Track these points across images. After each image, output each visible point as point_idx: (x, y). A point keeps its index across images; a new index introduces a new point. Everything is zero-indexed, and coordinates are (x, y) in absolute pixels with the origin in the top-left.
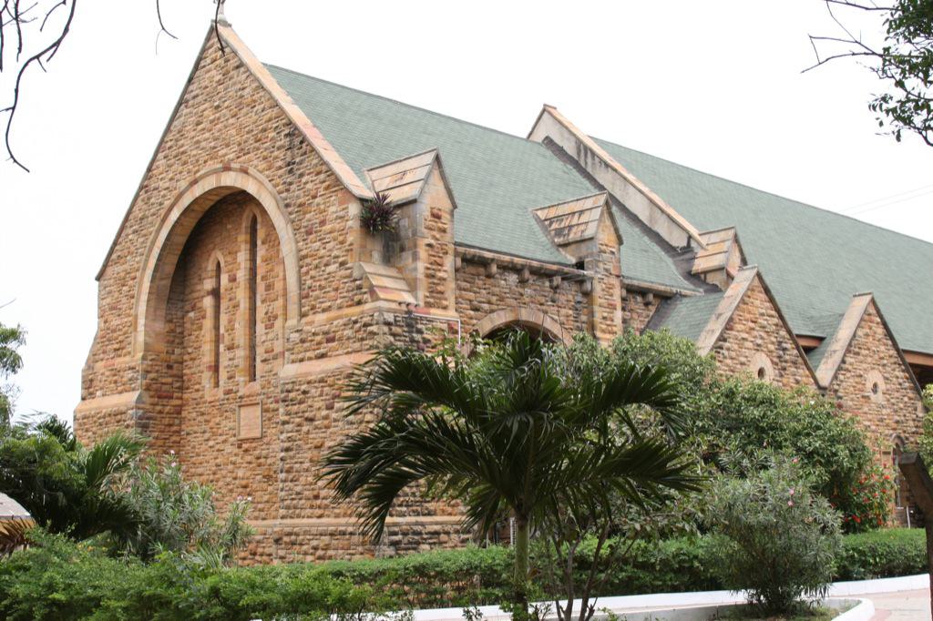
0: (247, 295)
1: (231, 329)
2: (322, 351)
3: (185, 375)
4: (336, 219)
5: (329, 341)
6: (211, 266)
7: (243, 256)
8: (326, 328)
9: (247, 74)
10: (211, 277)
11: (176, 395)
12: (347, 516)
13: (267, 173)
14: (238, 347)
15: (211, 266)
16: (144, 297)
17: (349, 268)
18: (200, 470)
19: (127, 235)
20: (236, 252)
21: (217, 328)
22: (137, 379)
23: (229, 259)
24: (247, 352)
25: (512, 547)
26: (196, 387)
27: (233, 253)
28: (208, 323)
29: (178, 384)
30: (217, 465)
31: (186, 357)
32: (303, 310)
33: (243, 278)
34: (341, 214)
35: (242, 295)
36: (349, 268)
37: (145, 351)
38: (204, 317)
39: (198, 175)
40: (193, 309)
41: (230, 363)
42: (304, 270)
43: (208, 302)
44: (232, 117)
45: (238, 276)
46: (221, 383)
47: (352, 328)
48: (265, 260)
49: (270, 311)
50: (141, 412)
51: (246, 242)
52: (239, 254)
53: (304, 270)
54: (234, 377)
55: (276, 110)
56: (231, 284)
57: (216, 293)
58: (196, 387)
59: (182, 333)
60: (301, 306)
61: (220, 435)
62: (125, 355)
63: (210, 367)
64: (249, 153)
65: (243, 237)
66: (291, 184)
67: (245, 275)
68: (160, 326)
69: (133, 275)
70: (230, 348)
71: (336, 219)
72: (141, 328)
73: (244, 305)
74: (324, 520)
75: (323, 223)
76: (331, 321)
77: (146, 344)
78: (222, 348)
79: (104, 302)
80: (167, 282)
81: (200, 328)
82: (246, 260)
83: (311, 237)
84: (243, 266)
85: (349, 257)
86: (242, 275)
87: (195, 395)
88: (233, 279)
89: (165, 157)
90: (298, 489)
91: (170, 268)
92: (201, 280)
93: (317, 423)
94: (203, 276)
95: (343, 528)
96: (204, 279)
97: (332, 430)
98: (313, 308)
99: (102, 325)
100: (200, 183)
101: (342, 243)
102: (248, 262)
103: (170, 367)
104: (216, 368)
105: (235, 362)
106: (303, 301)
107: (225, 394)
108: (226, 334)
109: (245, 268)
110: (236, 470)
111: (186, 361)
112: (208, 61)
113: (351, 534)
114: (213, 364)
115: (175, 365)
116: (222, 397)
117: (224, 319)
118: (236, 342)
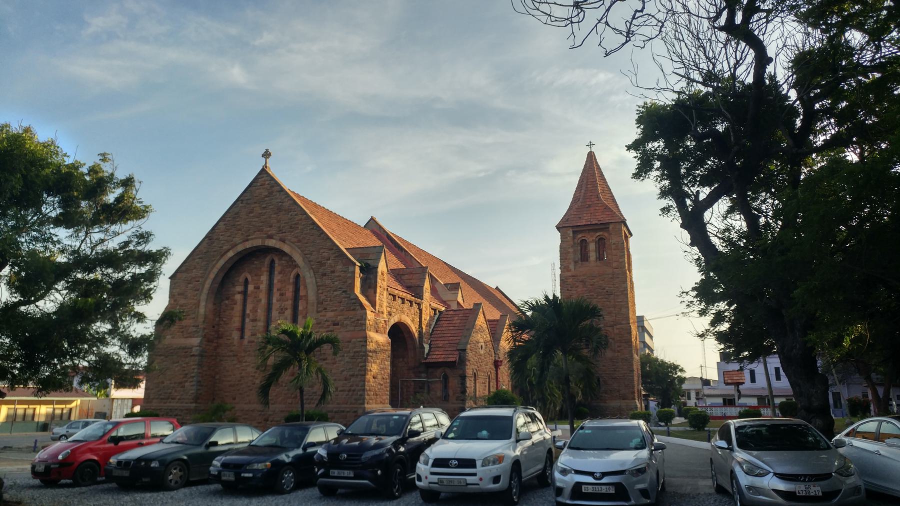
1: (255, 310)
6: (241, 279)
7: (264, 278)
12: (172, 432)
13: (297, 244)
14: (259, 321)
15: (241, 279)
16: (205, 291)
19: (194, 259)
20: (261, 275)
21: (244, 310)
22: (199, 332)
23: (255, 278)
25: (409, 427)
27: (258, 276)
28: (238, 308)
30: (241, 377)
31: (221, 322)
38: (235, 304)
39: (249, 238)
40: (227, 299)
42: (320, 291)
43: (239, 297)
45: (261, 287)
51: (267, 271)
52: (262, 277)
53: (320, 291)
55: (304, 216)
56: (256, 290)
57: (245, 293)
60: (318, 307)
64: (285, 233)
65: (265, 269)
66: (313, 251)
68: (211, 306)
69: (197, 279)
70: (254, 320)
73: (264, 301)
75: (333, 272)
77: (205, 315)
78: (247, 320)
79: (174, 291)
80: (217, 285)
81: (233, 309)
84: (265, 282)
86: (264, 286)
88: (257, 288)
90: (315, 390)
92: (234, 286)
94: (236, 284)
97: (337, 365)
99: (172, 302)
112: (259, 184)
113: (348, 412)
114: (240, 327)
117: (249, 307)
118: (258, 318)
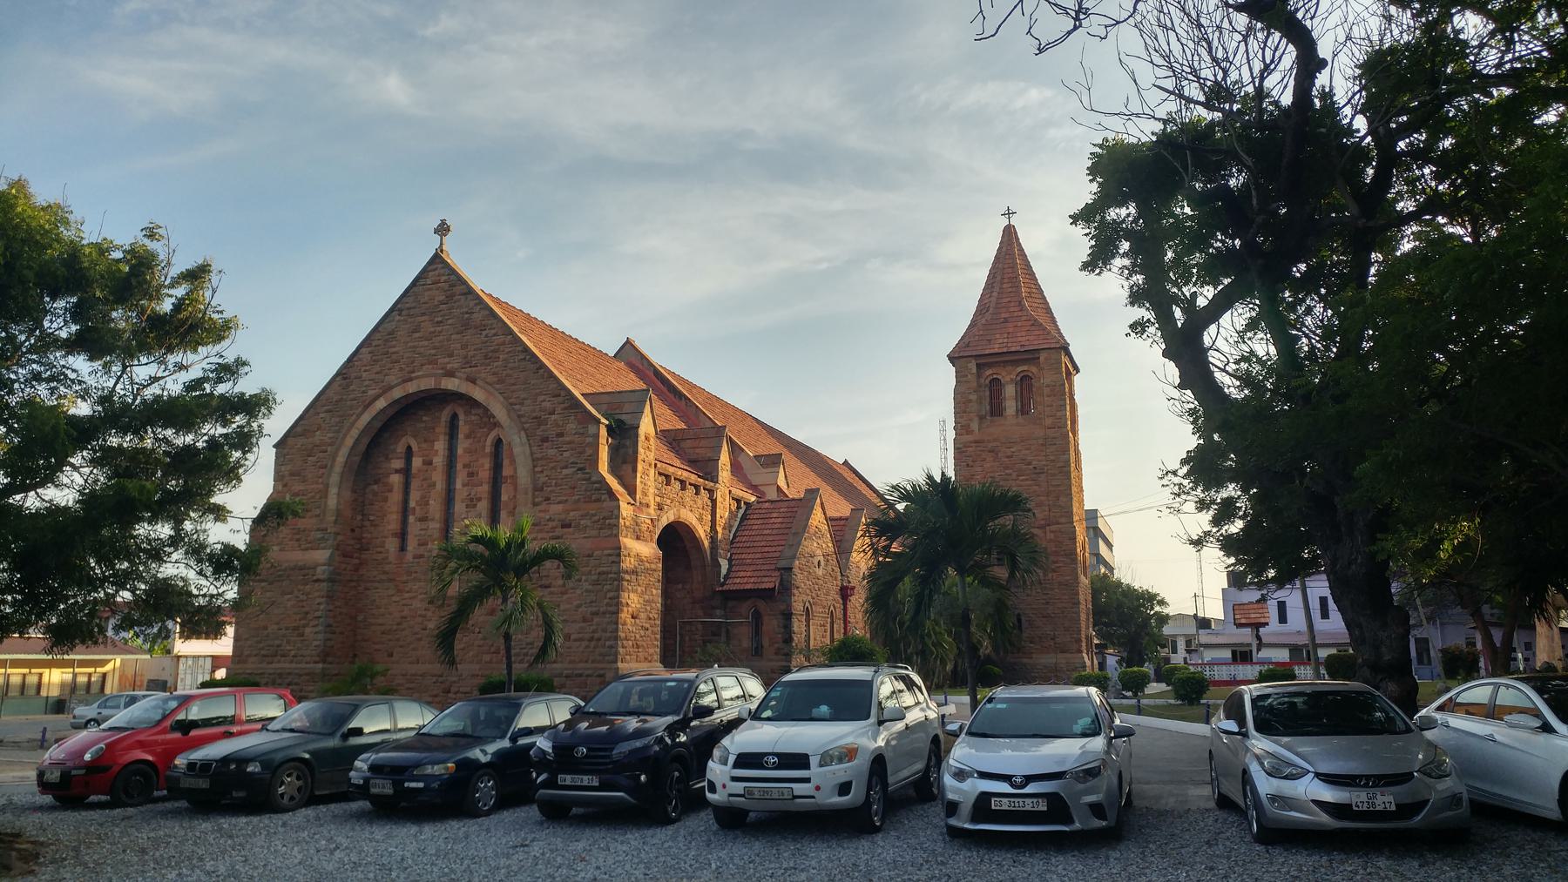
0: (445, 477)
1: (424, 502)
2: (556, 534)
3: (363, 538)
4: (575, 434)
5: (563, 526)
7: (441, 445)
8: (563, 516)
9: (477, 301)
10: (401, 458)
11: (356, 555)
13: (498, 386)
16: (338, 468)
17: (587, 473)
18: (380, 621)
20: (434, 441)
21: (406, 501)
23: (424, 445)
24: (443, 526)
26: (379, 549)
27: (430, 442)
29: (358, 546)
32: (536, 500)
33: (441, 464)
34: (581, 431)
35: (438, 478)
36: (587, 473)
37: (337, 516)
38: (390, 491)
39: (413, 375)
40: (376, 482)
41: (423, 532)
43: (396, 479)
44: (458, 333)
46: (410, 548)
47: (590, 519)
48: (468, 451)
49: (473, 494)
50: (331, 568)
51: (445, 434)
54: (427, 544)
57: (406, 472)
58: (379, 549)
59: (363, 502)
61: (408, 592)
62: (311, 517)
63: (395, 535)
65: (442, 428)
67: (443, 462)
68: (347, 494)
71: (575, 434)
72: (333, 491)
74: (273, 666)
75: (561, 435)
76: (567, 512)
78: (411, 519)
80: (357, 459)
81: (386, 500)
82: (444, 449)
83: (545, 444)
85: (587, 465)
86: (439, 460)
87: (380, 557)
89: (369, 353)
91: (362, 447)
92: (388, 459)
93: (552, 589)
95: (580, 672)
96: (392, 459)
98: (548, 499)
100: (414, 381)
101: (581, 453)
102: (446, 451)
103: (353, 530)
104: (402, 535)
105: (429, 533)
106: (536, 493)
107: (414, 558)
108: (418, 508)
109: (444, 455)
110: (425, 623)
111: (366, 527)
115: (356, 529)
116: (411, 560)
